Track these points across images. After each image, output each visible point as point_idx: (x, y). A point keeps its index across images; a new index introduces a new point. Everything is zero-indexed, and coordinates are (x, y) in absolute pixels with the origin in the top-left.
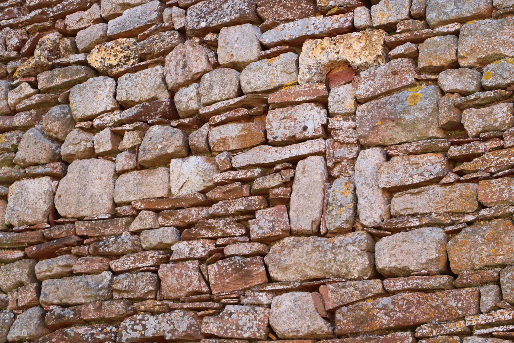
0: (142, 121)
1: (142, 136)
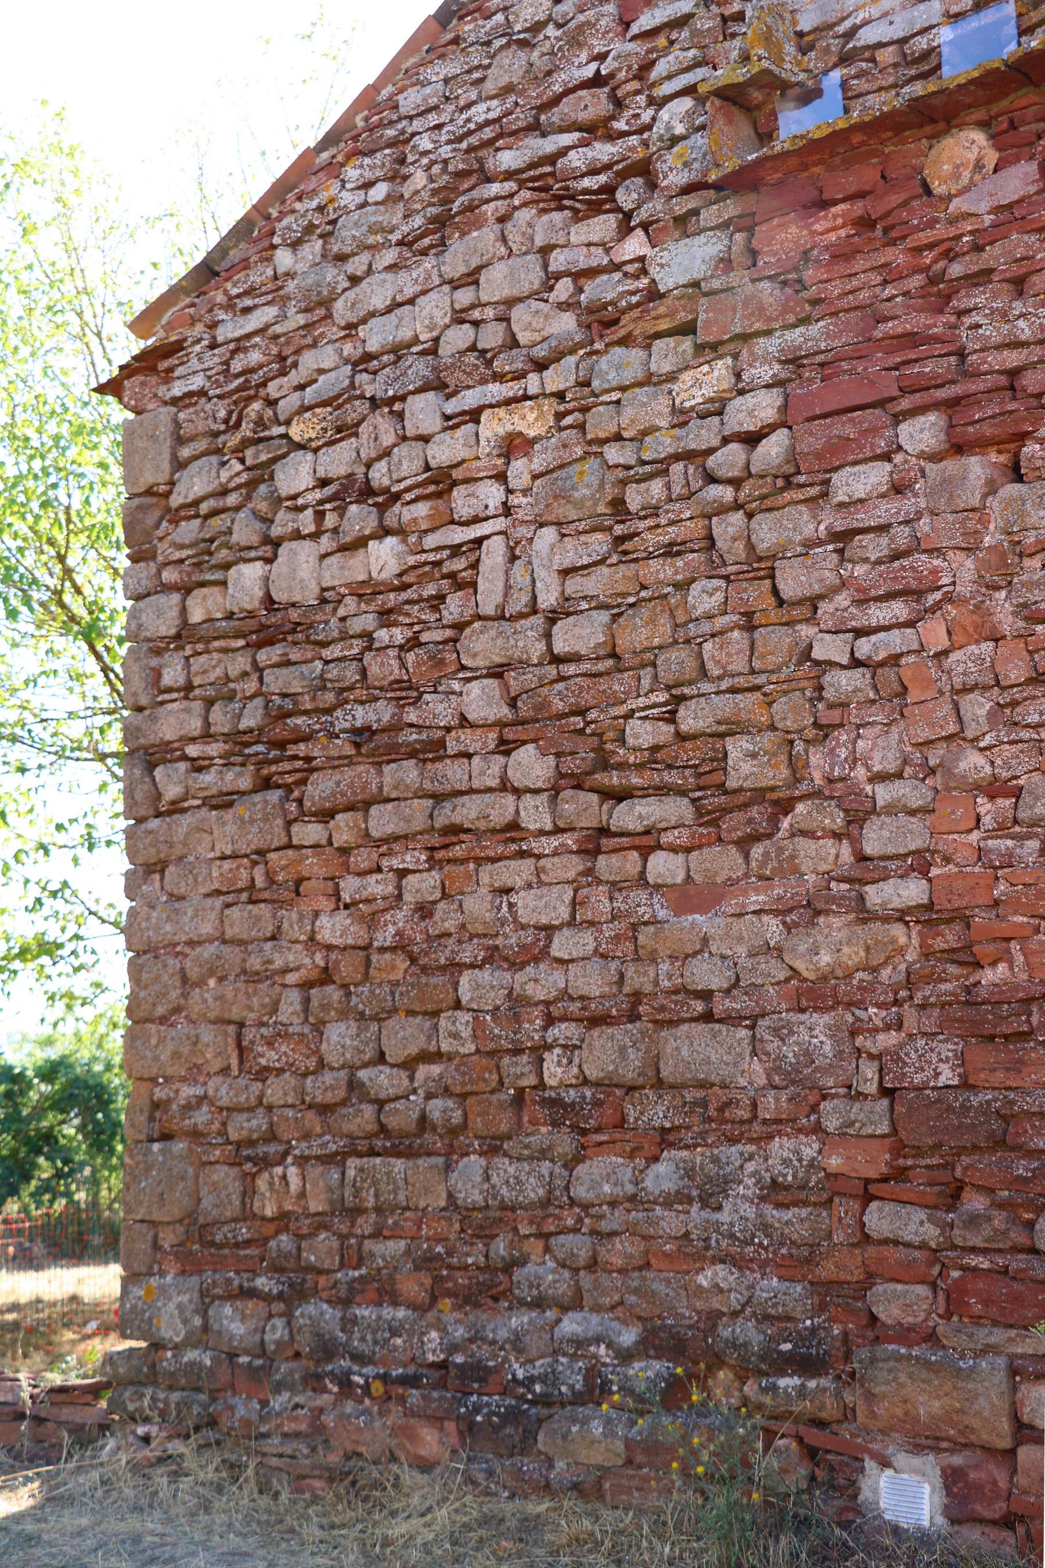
0: (340, 500)
1: (342, 516)
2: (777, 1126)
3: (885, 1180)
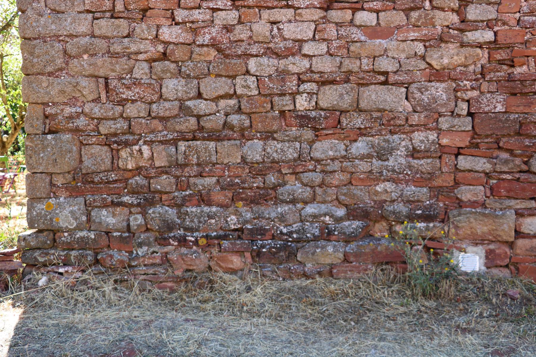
2: (415, 128)
3: (467, 147)
